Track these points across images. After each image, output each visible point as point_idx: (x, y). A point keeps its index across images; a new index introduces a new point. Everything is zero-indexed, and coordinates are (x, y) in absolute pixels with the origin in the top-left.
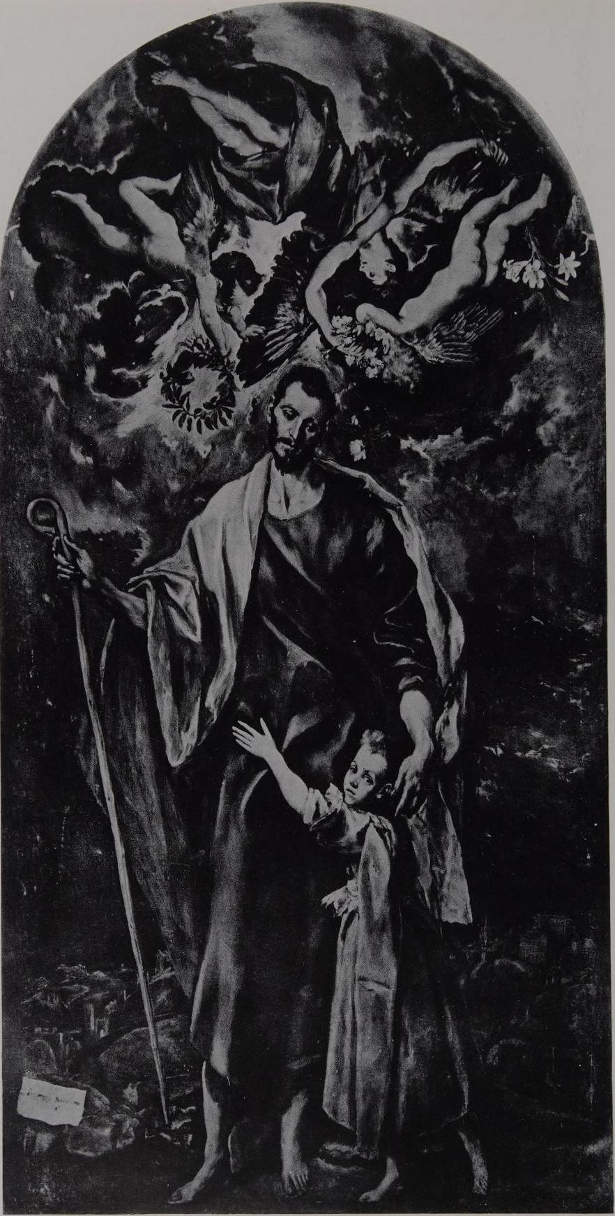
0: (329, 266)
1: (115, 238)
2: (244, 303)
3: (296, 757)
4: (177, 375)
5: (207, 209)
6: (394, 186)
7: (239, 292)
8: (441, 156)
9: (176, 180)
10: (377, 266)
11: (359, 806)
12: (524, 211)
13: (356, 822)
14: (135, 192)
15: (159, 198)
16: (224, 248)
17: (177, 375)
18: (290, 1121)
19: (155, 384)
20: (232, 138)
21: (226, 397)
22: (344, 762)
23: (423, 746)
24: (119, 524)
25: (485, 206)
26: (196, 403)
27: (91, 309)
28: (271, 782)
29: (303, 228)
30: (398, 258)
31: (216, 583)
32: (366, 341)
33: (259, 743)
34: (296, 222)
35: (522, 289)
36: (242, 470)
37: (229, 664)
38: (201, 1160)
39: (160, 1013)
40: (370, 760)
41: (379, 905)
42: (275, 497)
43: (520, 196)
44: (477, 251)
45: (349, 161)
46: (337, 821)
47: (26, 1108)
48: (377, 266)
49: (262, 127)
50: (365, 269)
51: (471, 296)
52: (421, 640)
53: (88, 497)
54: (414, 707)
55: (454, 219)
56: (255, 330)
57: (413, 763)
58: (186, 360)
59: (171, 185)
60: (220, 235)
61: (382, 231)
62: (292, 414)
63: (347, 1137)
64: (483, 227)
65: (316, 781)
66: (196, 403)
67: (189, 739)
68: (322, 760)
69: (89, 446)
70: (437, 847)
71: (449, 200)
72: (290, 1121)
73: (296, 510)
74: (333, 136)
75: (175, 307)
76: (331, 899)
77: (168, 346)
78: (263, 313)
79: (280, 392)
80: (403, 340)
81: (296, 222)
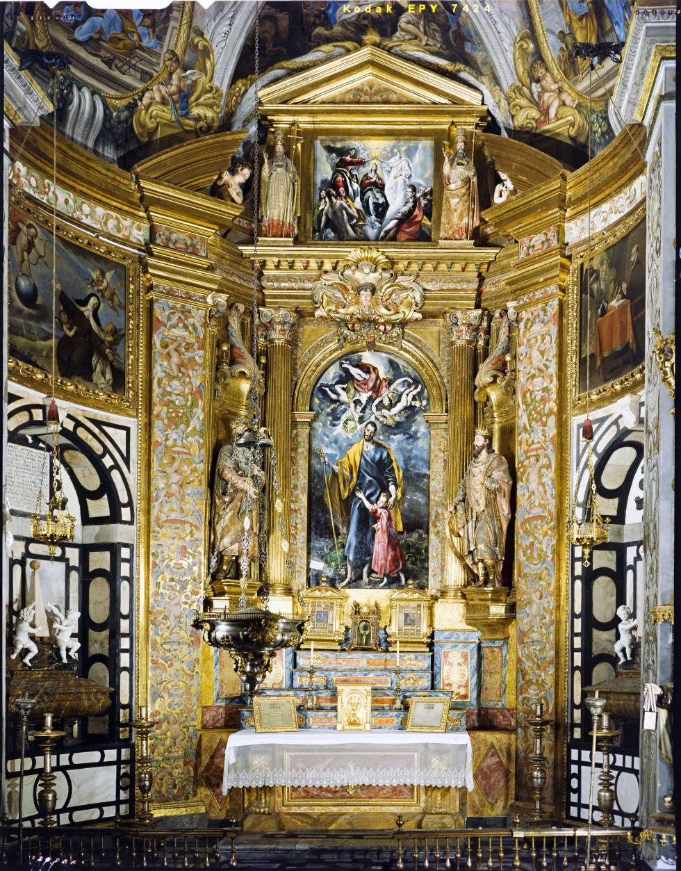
0: (376, 402)
1: (334, 397)
2: (359, 409)
3: (368, 498)
4: (346, 422)
10: (386, 402)
12: (415, 392)
13: (380, 511)
14: (338, 388)
15: (343, 389)
17: (346, 422)
18: (365, 570)
20: (357, 377)
21: (355, 428)
22: (378, 499)
23: (394, 496)
28: (363, 503)
29: (613, 818)
30: (391, 401)
32: (384, 416)
34: (370, 393)
37: (355, 480)
39: (339, 548)
40: (383, 499)
43: (416, 388)
46: (376, 511)
47: (312, 566)
48: (386, 402)
49: (364, 375)
51: (406, 408)
52: (76, 726)
53: (327, 446)
54: (392, 488)
59: (345, 386)
60: (354, 396)
63: (376, 573)
65: (372, 503)
67: (346, 494)
68: (373, 498)
69: (328, 436)
70: (396, 516)
71: (401, 389)
72: (365, 570)
74: (378, 377)
75: (345, 410)
76: (375, 526)
77: (344, 418)
78: (363, 410)
80: (391, 417)
81: (370, 393)
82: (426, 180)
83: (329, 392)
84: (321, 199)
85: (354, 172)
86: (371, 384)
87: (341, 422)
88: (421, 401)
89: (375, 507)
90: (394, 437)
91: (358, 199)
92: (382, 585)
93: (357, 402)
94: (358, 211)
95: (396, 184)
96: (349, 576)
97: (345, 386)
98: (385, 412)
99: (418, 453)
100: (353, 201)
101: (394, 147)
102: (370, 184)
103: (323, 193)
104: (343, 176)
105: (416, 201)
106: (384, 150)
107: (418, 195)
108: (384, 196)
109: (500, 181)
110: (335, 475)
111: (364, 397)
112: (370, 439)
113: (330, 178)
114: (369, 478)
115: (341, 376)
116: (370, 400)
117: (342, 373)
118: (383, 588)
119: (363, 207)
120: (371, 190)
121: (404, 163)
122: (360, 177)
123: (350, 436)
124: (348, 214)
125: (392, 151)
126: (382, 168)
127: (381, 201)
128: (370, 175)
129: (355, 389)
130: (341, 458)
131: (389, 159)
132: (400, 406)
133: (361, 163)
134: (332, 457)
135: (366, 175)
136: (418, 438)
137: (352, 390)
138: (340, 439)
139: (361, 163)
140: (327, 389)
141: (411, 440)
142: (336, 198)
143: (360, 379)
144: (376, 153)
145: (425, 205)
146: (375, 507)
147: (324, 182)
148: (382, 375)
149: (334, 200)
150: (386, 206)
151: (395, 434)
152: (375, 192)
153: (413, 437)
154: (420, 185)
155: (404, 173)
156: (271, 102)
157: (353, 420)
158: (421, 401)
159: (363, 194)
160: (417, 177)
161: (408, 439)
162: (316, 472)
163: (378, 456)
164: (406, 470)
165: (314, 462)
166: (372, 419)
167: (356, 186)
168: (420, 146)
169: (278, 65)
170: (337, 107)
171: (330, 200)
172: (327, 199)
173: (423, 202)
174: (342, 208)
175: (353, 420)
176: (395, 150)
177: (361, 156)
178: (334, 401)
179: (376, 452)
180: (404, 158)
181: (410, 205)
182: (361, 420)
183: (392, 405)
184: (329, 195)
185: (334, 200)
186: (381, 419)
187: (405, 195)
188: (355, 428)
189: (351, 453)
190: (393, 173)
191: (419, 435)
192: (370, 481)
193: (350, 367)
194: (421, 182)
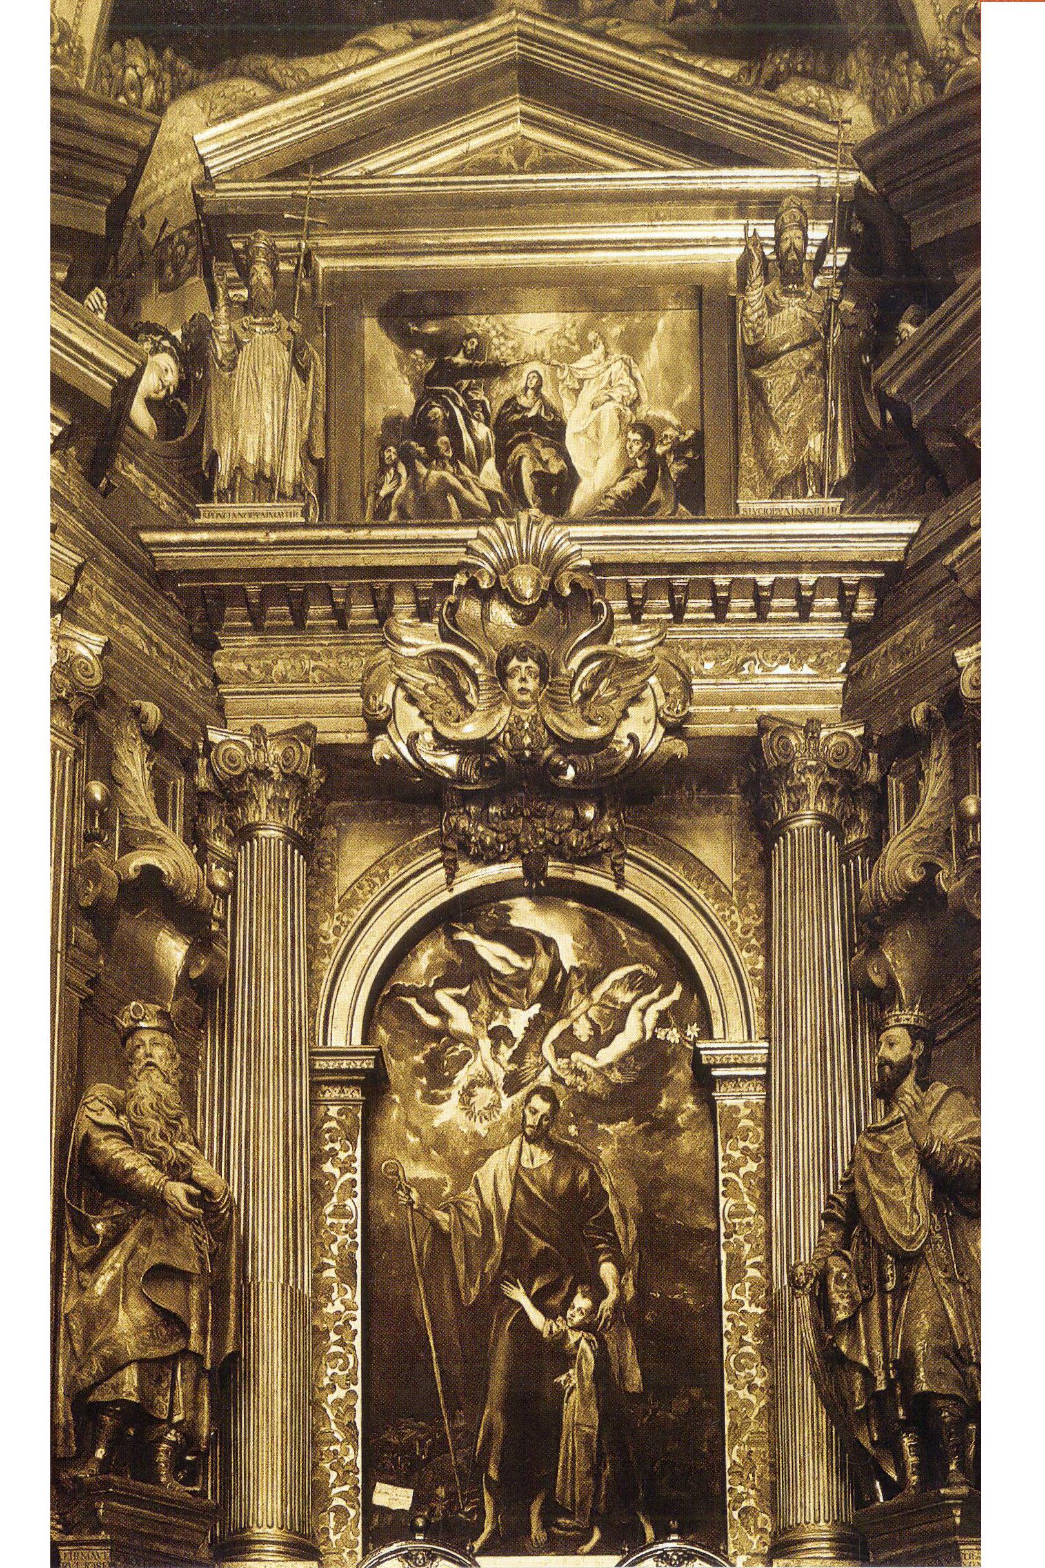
1: (432, 1021)
2: (506, 1052)
5: (484, 1004)
6: (590, 990)
7: (503, 1048)
10: (583, 1031)
11: (576, 1328)
12: (665, 1003)
13: (574, 1337)
14: (444, 997)
15: (459, 999)
16: (494, 1024)
19: (455, 1097)
20: (497, 965)
21: (495, 1106)
22: (567, 1303)
23: (613, 1295)
24: (434, 1174)
27: (419, 1059)
28: (523, 1313)
30: (595, 1027)
32: (578, 1072)
33: (518, 1295)
34: (536, 1009)
40: (581, 1302)
42: (525, 1156)
44: (639, 1024)
45: (566, 977)
46: (564, 1336)
48: (583, 1031)
49: (516, 960)
50: (577, 1033)
53: (415, 1159)
54: (607, 1271)
55: (627, 1008)
56: (512, 1067)
58: (472, 1084)
59: (464, 992)
60: (492, 1017)
61: (586, 1012)
63: (570, 1515)
64: (643, 1011)
65: (549, 1314)
66: (478, 1107)
67: (474, 1292)
68: (555, 1302)
69: (417, 1132)
73: (537, 1164)
74: (557, 965)
77: (462, 1078)
78: (518, 1057)
79: (528, 1099)
80: (599, 1071)
81: (536, 1009)
82: (681, 411)
83: (420, 1011)
84: (383, 469)
85: (479, 396)
86: (537, 985)
87: (455, 1092)
88: (682, 1029)
89: (558, 1326)
90: (610, 1129)
91: (490, 465)
92: (587, 1548)
93: (500, 1036)
94: (490, 494)
95: (597, 423)
96: (488, 1527)
97: (464, 992)
98: (580, 1059)
99: (679, 1170)
100: (477, 471)
101: (587, 327)
102: (525, 423)
103: (391, 453)
104: (447, 407)
105: (655, 465)
106: (561, 335)
107: (660, 450)
108: (563, 454)
109: (940, 869)
110: (440, 1236)
111: (518, 1021)
112: (540, 1136)
113: (408, 412)
114: (539, 1244)
115: (450, 964)
116: (537, 1028)
117: (451, 954)
118: (592, 1552)
119: (505, 483)
120: (527, 439)
121: (617, 368)
122: (495, 407)
123: (481, 1128)
124: (462, 503)
125: (582, 340)
126: (556, 383)
127: (555, 467)
128: (524, 401)
129: (492, 997)
130: (459, 1187)
131: (576, 357)
132: (622, 1044)
133: (498, 370)
134: (430, 1188)
135: (511, 402)
136: (679, 1130)
137: (484, 1004)
138: (455, 1141)
139: (498, 370)
140: (412, 1001)
141: (657, 1136)
142: (427, 463)
143: (507, 971)
144: (539, 344)
145: (681, 475)
146: (558, 1326)
147: (392, 424)
148: (569, 959)
149: (423, 470)
150: (569, 480)
151: (610, 1122)
152: (538, 446)
153: (665, 1127)
154: (665, 424)
155: (617, 394)
156: (235, 173)
157: (491, 1083)
158: (682, 1029)
159: (503, 453)
160: (657, 403)
161: (648, 1132)
162: (386, 1230)
163: (563, 1182)
164: (646, 1222)
165: (380, 1202)
166: (545, 1078)
167: (483, 431)
168: (661, 324)
169: (252, 62)
170: (426, 180)
171: (412, 470)
172: (402, 469)
173: (675, 468)
174: (445, 488)
175: (491, 1083)
176: (592, 336)
177: (500, 351)
178: (437, 1034)
179: (557, 1171)
180: (616, 354)
181: (638, 475)
182: (512, 1084)
183: (600, 1041)
184: (406, 457)
185: (423, 470)
186: (569, 1079)
187: (625, 452)
188: (495, 1106)
189: (485, 1175)
190: (589, 393)
191: (680, 1119)
192: (543, 1252)
193: (476, 940)
194: (669, 416)
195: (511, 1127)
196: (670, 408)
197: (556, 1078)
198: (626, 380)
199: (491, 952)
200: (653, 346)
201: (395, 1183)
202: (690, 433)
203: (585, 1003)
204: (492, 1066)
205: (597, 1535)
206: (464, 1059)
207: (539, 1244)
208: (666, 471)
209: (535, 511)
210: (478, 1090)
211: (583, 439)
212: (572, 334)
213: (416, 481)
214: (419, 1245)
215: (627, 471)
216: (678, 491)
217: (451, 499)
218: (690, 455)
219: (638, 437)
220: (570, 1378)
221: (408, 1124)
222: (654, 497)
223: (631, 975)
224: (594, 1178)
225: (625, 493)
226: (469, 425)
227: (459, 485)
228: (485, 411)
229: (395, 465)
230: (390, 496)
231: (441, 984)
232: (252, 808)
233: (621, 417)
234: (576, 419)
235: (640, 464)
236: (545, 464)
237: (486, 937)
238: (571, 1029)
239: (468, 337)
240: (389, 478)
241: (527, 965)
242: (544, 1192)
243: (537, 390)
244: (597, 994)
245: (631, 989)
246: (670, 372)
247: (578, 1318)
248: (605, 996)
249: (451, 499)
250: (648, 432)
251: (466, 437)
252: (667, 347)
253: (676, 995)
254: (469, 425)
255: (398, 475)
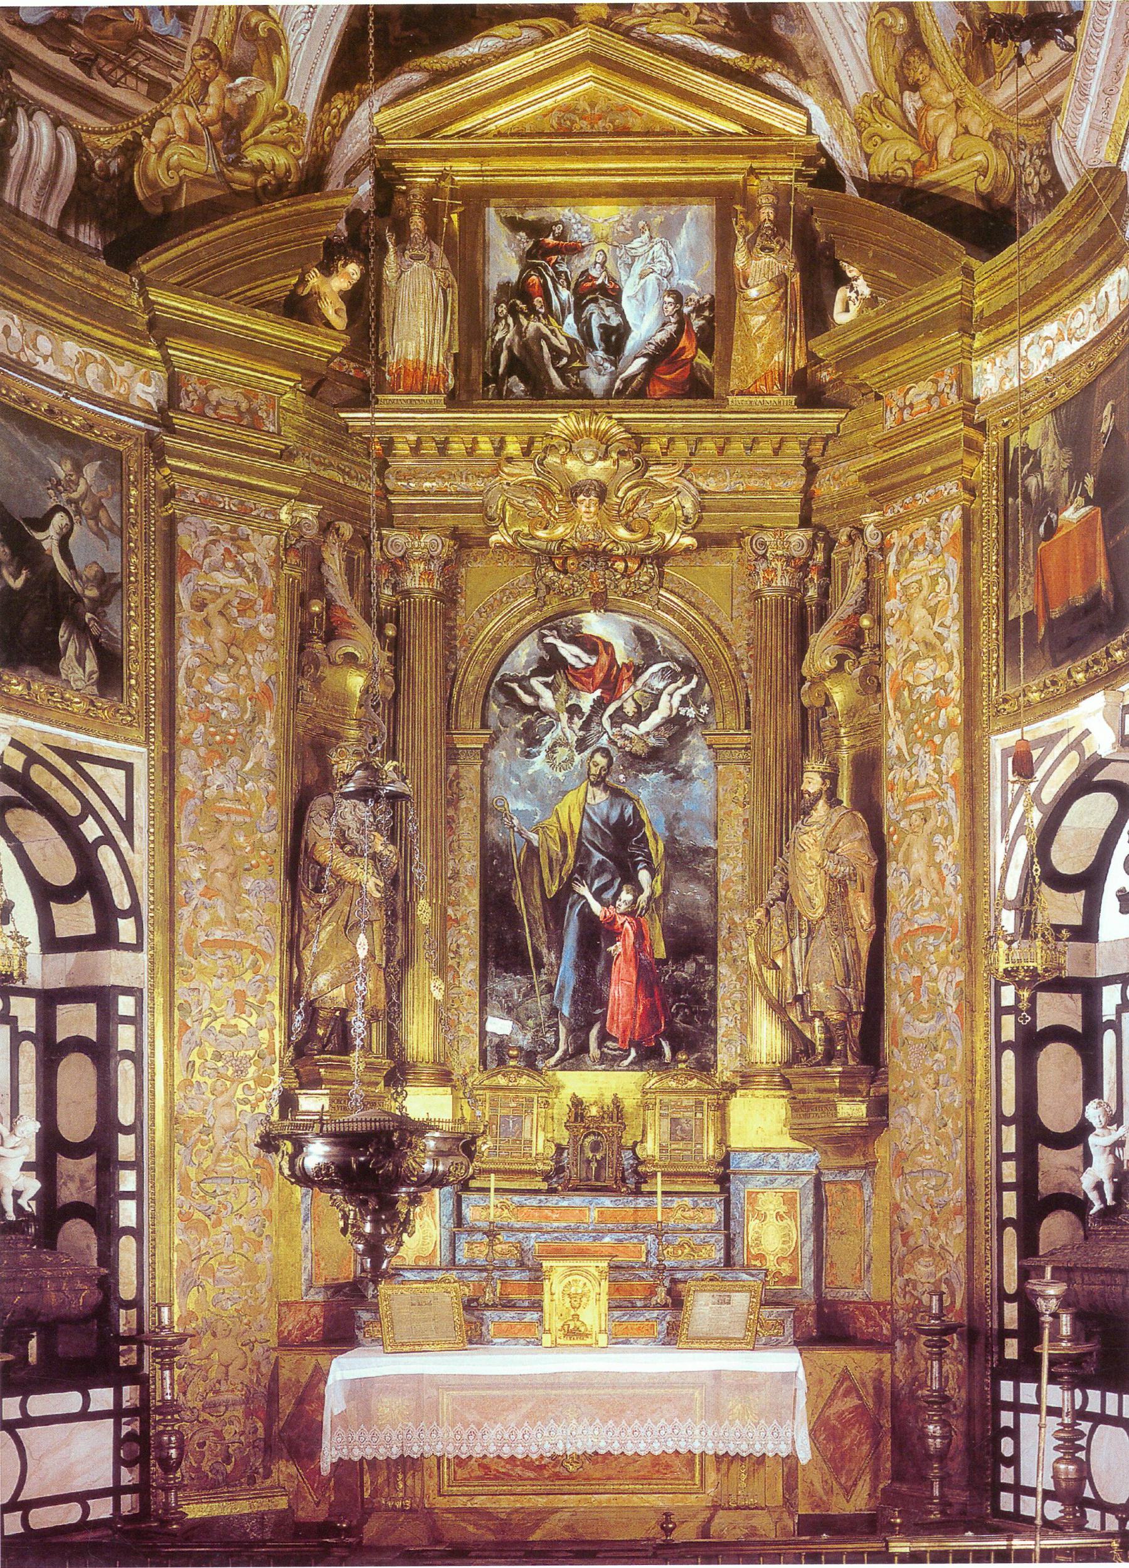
1: (528, 700)
2: (578, 722)
3: (597, 895)
4: (552, 750)
5: (564, 689)
6: (636, 678)
7: (576, 719)
8: (655, 668)
9: (123, 1433)
10: (630, 709)
11: (623, 914)
12: (685, 690)
13: (620, 920)
14: (536, 683)
15: (546, 685)
17: (552, 750)
18: (594, 1033)
19: (543, 754)
20: (572, 660)
21: (571, 760)
22: (616, 896)
24: (529, 808)
25: (673, 686)
26: (558, 761)
27: (519, 726)
28: (587, 904)
30: (638, 706)
31: (566, 827)
32: (625, 737)
33: (584, 891)
34: (598, 693)
35: (687, 718)
36: (577, 787)
38: (557, 1049)
40: (626, 896)
41: (630, 951)
43: (687, 682)
45: (619, 670)
48: (630, 709)
49: (585, 658)
51: (669, 721)
53: (516, 796)
54: (644, 876)
55: (660, 693)
56: (581, 733)
57: (643, 899)
58: (554, 745)
59: (549, 679)
62: (596, 765)
64: (671, 695)
65: (603, 903)
66: (558, 761)
67: (555, 889)
69: (518, 778)
72: (594, 1033)
73: (598, 801)
77: (548, 740)
78: (586, 726)
79: (592, 757)
80: (641, 737)
81: (598, 693)
83: (520, 692)
84: (498, 319)
85: (563, 268)
86: (600, 676)
88: (698, 707)
91: (570, 319)
92: (626, 1063)
93: (574, 710)
95: (644, 289)
96: (562, 1047)
100: (561, 323)
103: (503, 309)
104: (541, 276)
105: (683, 322)
106: (620, 222)
107: (686, 310)
108: (620, 312)
110: (533, 852)
111: (586, 701)
112: (600, 782)
113: (514, 280)
114: (598, 857)
115: (542, 659)
116: (599, 706)
117: (543, 653)
120: (595, 300)
122: (574, 276)
126: (616, 258)
127: (615, 321)
128: (594, 273)
129: (570, 685)
132: (656, 718)
133: (576, 249)
136: (692, 779)
137: (564, 689)
139: (576, 249)
140: (515, 686)
141: (679, 783)
142: (527, 317)
143: (580, 665)
144: (603, 230)
147: (504, 287)
148: (621, 658)
149: (524, 322)
152: (603, 306)
157: (567, 744)
158: (698, 707)
159: (579, 307)
160: (685, 275)
161: (673, 780)
165: (492, 826)
166: (604, 741)
167: (565, 294)
171: (517, 321)
172: (510, 320)
173: (697, 323)
175: (567, 744)
176: (641, 223)
177: (578, 234)
181: (671, 328)
182: (582, 745)
183: (641, 716)
184: (513, 311)
189: (563, 809)
190: (638, 267)
193: (559, 643)
195: (580, 775)
196: (693, 276)
197: (612, 742)
198: (664, 258)
199: (569, 651)
200: (684, 232)
201: (502, 814)
202: (708, 297)
203: (632, 689)
204: (568, 731)
205: (633, 1053)
206: (550, 727)
207: (598, 857)
208: (690, 325)
209: (600, 353)
210: (558, 749)
211: (634, 301)
212: (627, 221)
213: (520, 331)
214: (518, 855)
215: (664, 324)
216: (698, 340)
217: (543, 343)
218: (706, 313)
219: (671, 300)
220: (616, 948)
221: (511, 772)
222: (681, 345)
223: (663, 669)
224: (635, 809)
225: (663, 342)
226: (556, 289)
227: (549, 333)
228: (567, 279)
229: (505, 318)
230: (502, 340)
231: (534, 673)
232: (409, 577)
233: (659, 285)
234: (629, 288)
235: (673, 320)
236: (608, 318)
237: (564, 641)
238: (621, 708)
239: (556, 224)
240: (501, 327)
241: (593, 661)
242: (603, 822)
243: (603, 265)
244: (639, 683)
245: (663, 679)
246: (694, 252)
247: (623, 908)
248: (645, 684)
249: (543, 343)
250: (678, 297)
251: (554, 298)
252: (693, 233)
253: (693, 684)
254: (556, 289)
255: (507, 325)
